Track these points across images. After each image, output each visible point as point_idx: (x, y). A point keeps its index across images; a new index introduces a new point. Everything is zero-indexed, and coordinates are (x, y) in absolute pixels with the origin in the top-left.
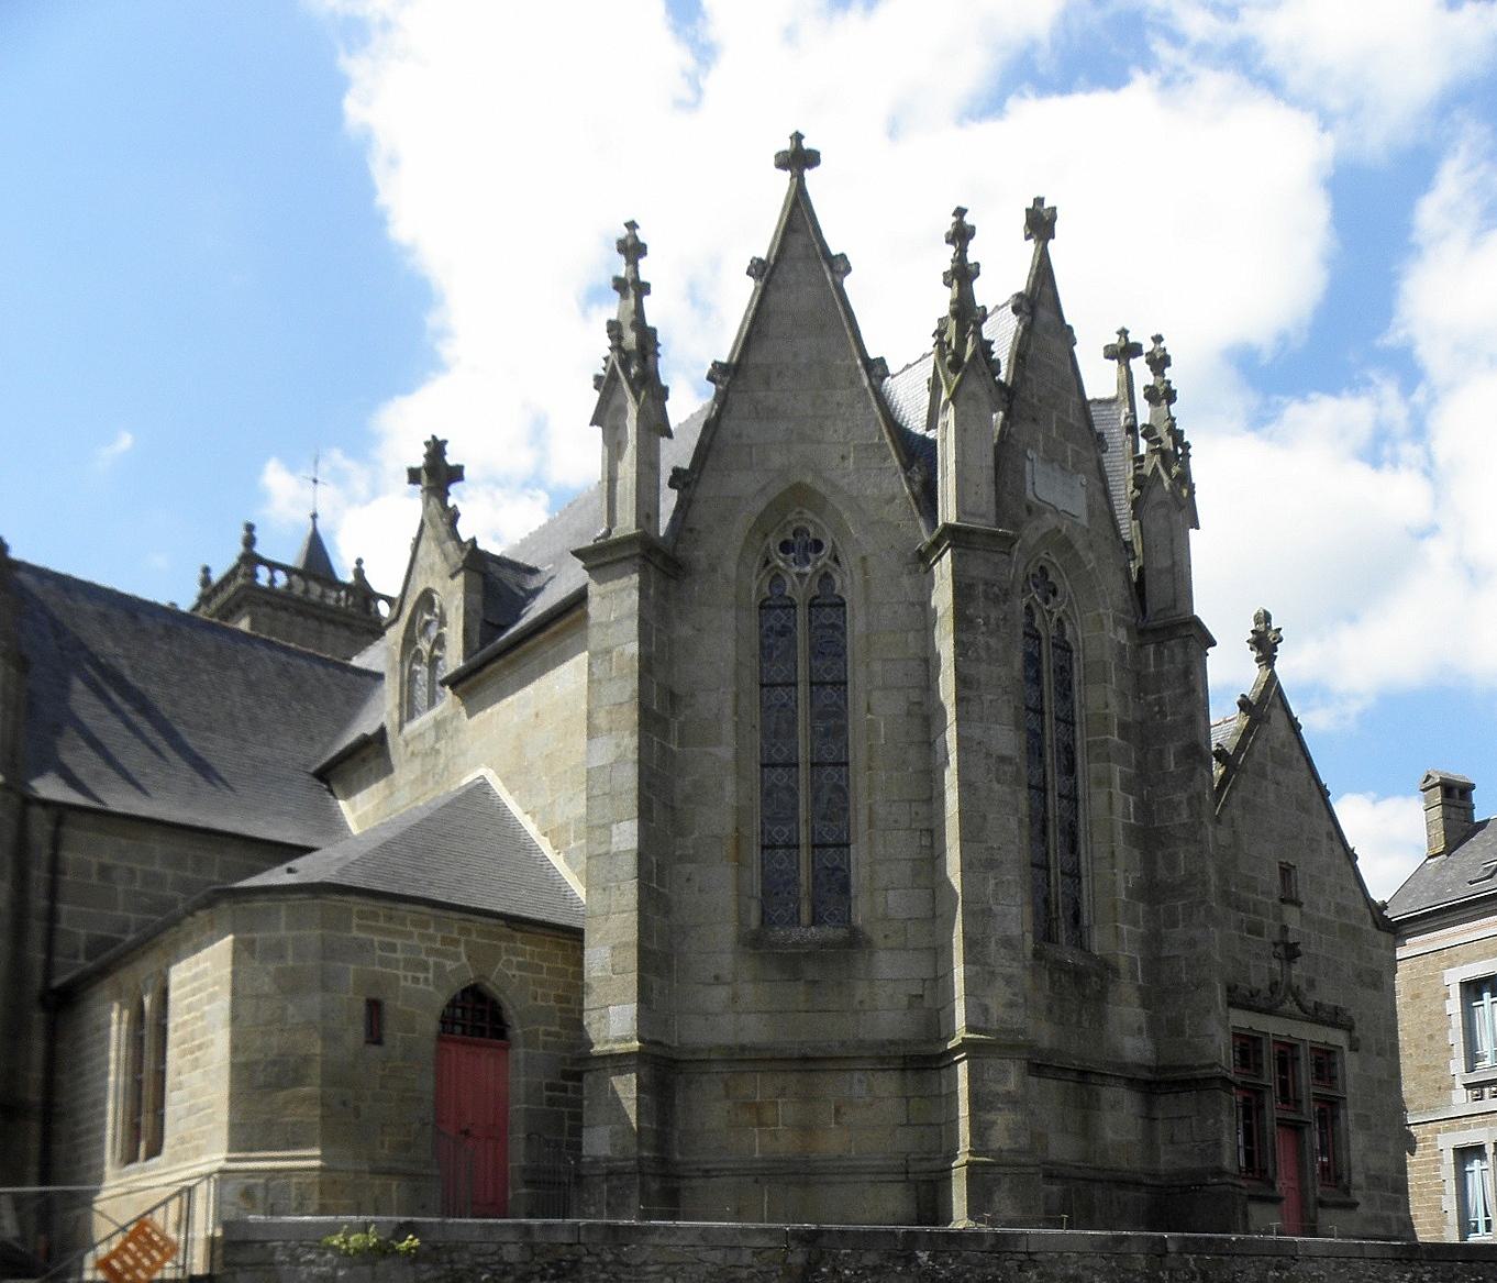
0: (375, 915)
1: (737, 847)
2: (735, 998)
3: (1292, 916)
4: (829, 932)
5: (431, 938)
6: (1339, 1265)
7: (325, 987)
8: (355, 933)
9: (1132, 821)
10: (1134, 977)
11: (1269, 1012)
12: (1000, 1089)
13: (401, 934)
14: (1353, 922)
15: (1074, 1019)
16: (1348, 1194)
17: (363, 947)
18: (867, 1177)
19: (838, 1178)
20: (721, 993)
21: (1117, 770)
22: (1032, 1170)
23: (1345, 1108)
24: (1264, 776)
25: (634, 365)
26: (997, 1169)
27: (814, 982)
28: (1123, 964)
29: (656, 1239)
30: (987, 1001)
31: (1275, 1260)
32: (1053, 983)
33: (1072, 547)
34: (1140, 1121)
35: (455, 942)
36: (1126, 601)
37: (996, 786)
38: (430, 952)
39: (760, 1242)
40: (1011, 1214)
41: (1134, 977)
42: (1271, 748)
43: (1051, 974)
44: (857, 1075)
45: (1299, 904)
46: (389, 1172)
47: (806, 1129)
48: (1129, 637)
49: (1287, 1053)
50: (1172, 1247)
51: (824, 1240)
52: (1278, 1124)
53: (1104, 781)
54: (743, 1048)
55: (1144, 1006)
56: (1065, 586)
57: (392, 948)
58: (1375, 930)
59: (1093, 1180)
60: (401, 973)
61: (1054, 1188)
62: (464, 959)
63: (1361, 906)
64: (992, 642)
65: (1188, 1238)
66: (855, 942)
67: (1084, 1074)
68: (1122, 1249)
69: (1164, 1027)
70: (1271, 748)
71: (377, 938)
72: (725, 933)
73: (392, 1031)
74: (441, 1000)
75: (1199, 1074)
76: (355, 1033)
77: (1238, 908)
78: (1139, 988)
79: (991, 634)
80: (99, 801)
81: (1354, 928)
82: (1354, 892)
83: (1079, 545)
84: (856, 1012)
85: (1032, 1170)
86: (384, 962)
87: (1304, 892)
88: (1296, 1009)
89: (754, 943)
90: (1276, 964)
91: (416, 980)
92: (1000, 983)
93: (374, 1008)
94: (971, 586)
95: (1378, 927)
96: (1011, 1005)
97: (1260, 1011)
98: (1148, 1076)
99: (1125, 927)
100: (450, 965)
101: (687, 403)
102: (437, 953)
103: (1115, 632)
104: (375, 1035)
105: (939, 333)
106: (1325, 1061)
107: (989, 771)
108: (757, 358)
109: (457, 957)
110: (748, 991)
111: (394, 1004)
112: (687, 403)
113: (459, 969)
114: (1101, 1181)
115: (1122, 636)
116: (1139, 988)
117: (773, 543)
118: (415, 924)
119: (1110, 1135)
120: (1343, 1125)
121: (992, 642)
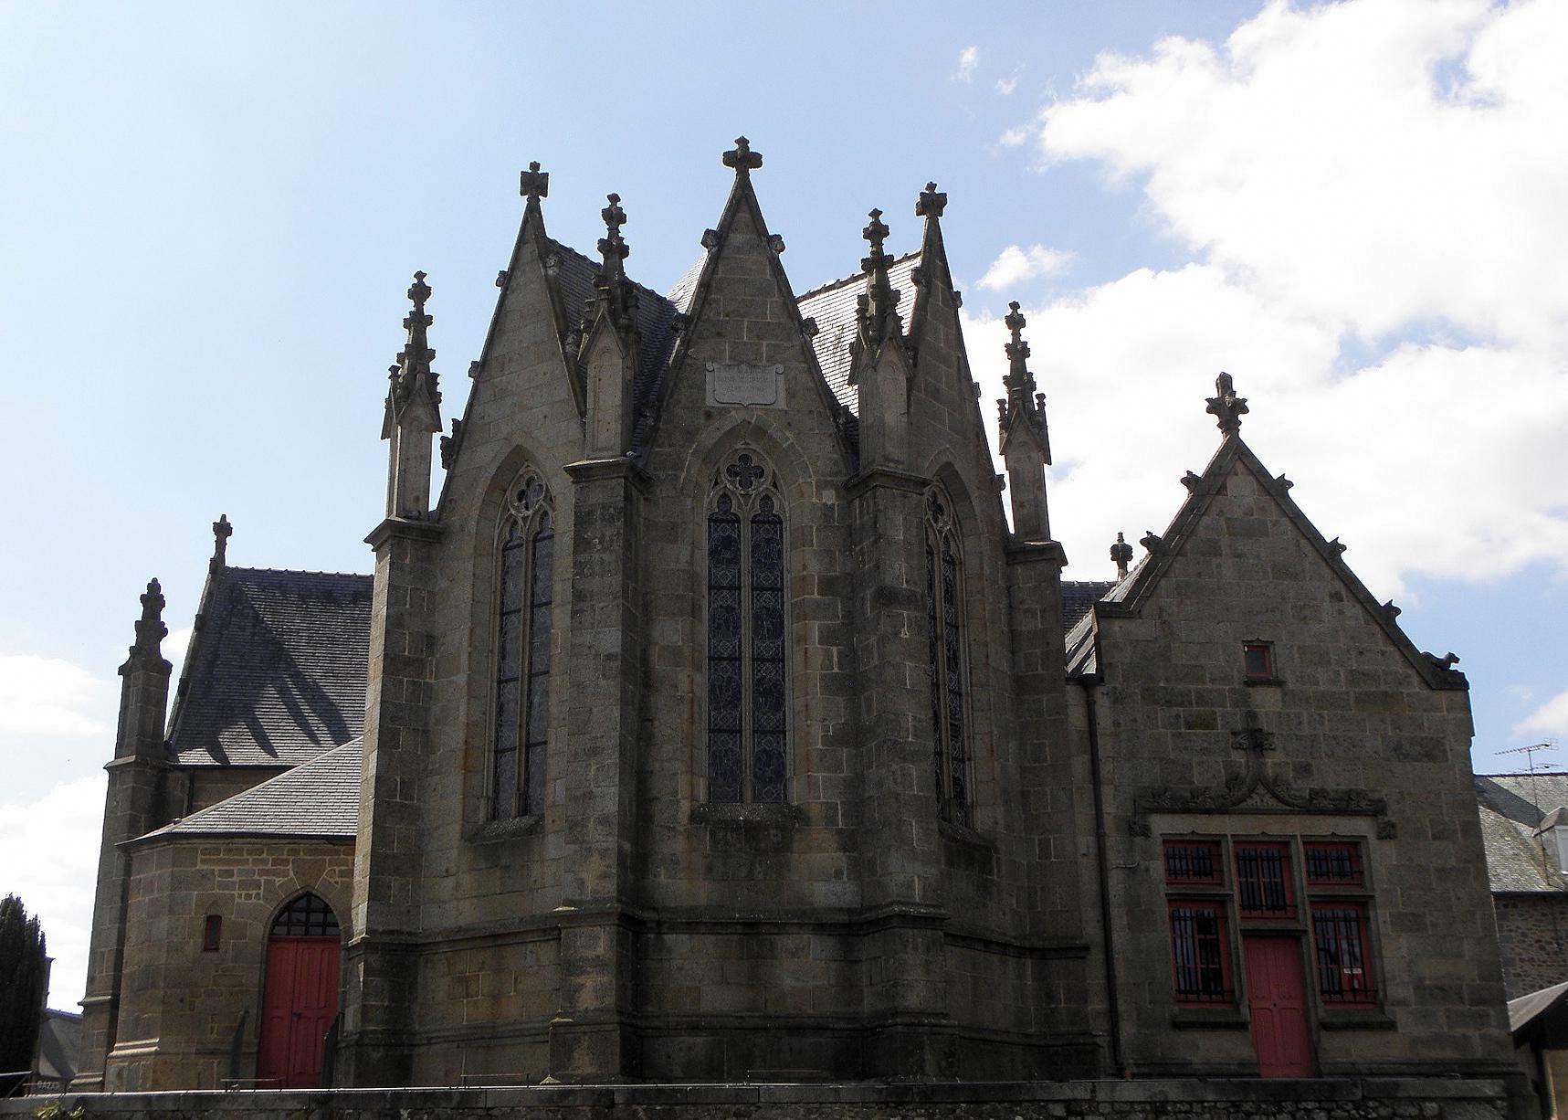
0: (217, 851)
1: (466, 757)
2: (457, 886)
3: (1267, 701)
4: (526, 821)
5: (264, 862)
6: (809, 1112)
7: (171, 912)
8: (200, 866)
9: (836, 670)
10: (831, 820)
11: (1222, 811)
12: (590, 954)
13: (238, 862)
14: (1383, 688)
15: (744, 872)
16: (1382, 1011)
17: (206, 876)
18: (528, 1039)
19: (508, 1041)
20: (449, 883)
21: (815, 627)
22: (611, 1027)
23: (1375, 908)
24: (1216, 552)
25: (412, 388)
26: (578, 1029)
27: (506, 868)
28: (815, 811)
29: (225, 1105)
30: (584, 875)
31: (734, 1108)
32: (714, 842)
33: (765, 432)
34: (833, 966)
35: (285, 862)
36: (836, 463)
37: (602, 682)
38: (262, 872)
39: (291, 1105)
40: (590, 1070)
41: (831, 820)
42: (1228, 520)
43: (713, 834)
44: (530, 946)
45: (1279, 684)
46: (213, 1053)
47: (496, 997)
48: (838, 496)
49: (1264, 858)
50: (618, 1099)
51: (334, 1104)
52: (1244, 937)
53: (802, 639)
54: (460, 929)
55: (844, 848)
56: (769, 466)
57: (231, 874)
58: (1426, 692)
59: (756, 1029)
60: (236, 893)
61: (699, 1040)
62: (292, 874)
63: (1398, 666)
64: (605, 556)
65: (635, 1090)
66: (535, 830)
67: (751, 927)
68: (566, 1103)
69: (862, 866)
70: (1228, 520)
71: (217, 868)
72: (455, 830)
73: (227, 939)
74: (270, 909)
75: (881, 913)
76: (194, 944)
77: (1169, 703)
78: (839, 832)
79: (605, 549)
80: (1298, 545)
81: (1386, 694)
82: (1383, 653)
83: (774, 428)
84: (531, 890)
85: (611, 1027)
86: (223, 886)
87: (1285, 662)
88: (1272, 803)
89: (472, 837)
90: (1238, 757)
91: (249, 896)
92: (596, 857)
93: (213, 922)
94: (590, 513)
95: (1429, 686)
96: (604, 876)
97: (1208, 812)
98: (843, 918)
99: (820, 775)
100: (279, 881)
101: (454, 400)
102: (268, 872)
103: (819, 495)
104: (211, 944)
105: (394, 369)
106: (1340, 859)
107: (596, 670)
108: (497, 352)
109: (285, 874)
110: (466, 879)
111: (229, 917)
112: (454, 400)
113: (287, 881)
114: (766, 1029)
115: (829, 497)
116: (839, 832)
117: (511, 495)
118: (250, 852)
119: (788, 982)
120: (1373, 926)
121: (605, 556)
